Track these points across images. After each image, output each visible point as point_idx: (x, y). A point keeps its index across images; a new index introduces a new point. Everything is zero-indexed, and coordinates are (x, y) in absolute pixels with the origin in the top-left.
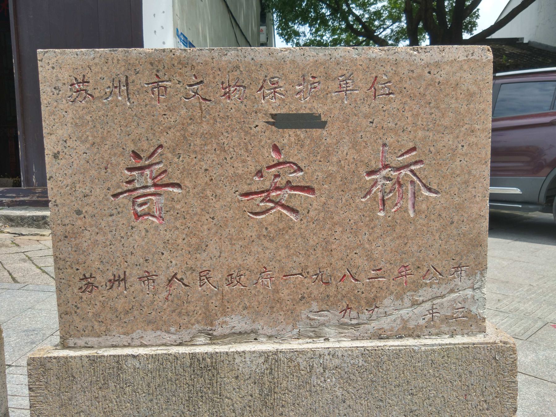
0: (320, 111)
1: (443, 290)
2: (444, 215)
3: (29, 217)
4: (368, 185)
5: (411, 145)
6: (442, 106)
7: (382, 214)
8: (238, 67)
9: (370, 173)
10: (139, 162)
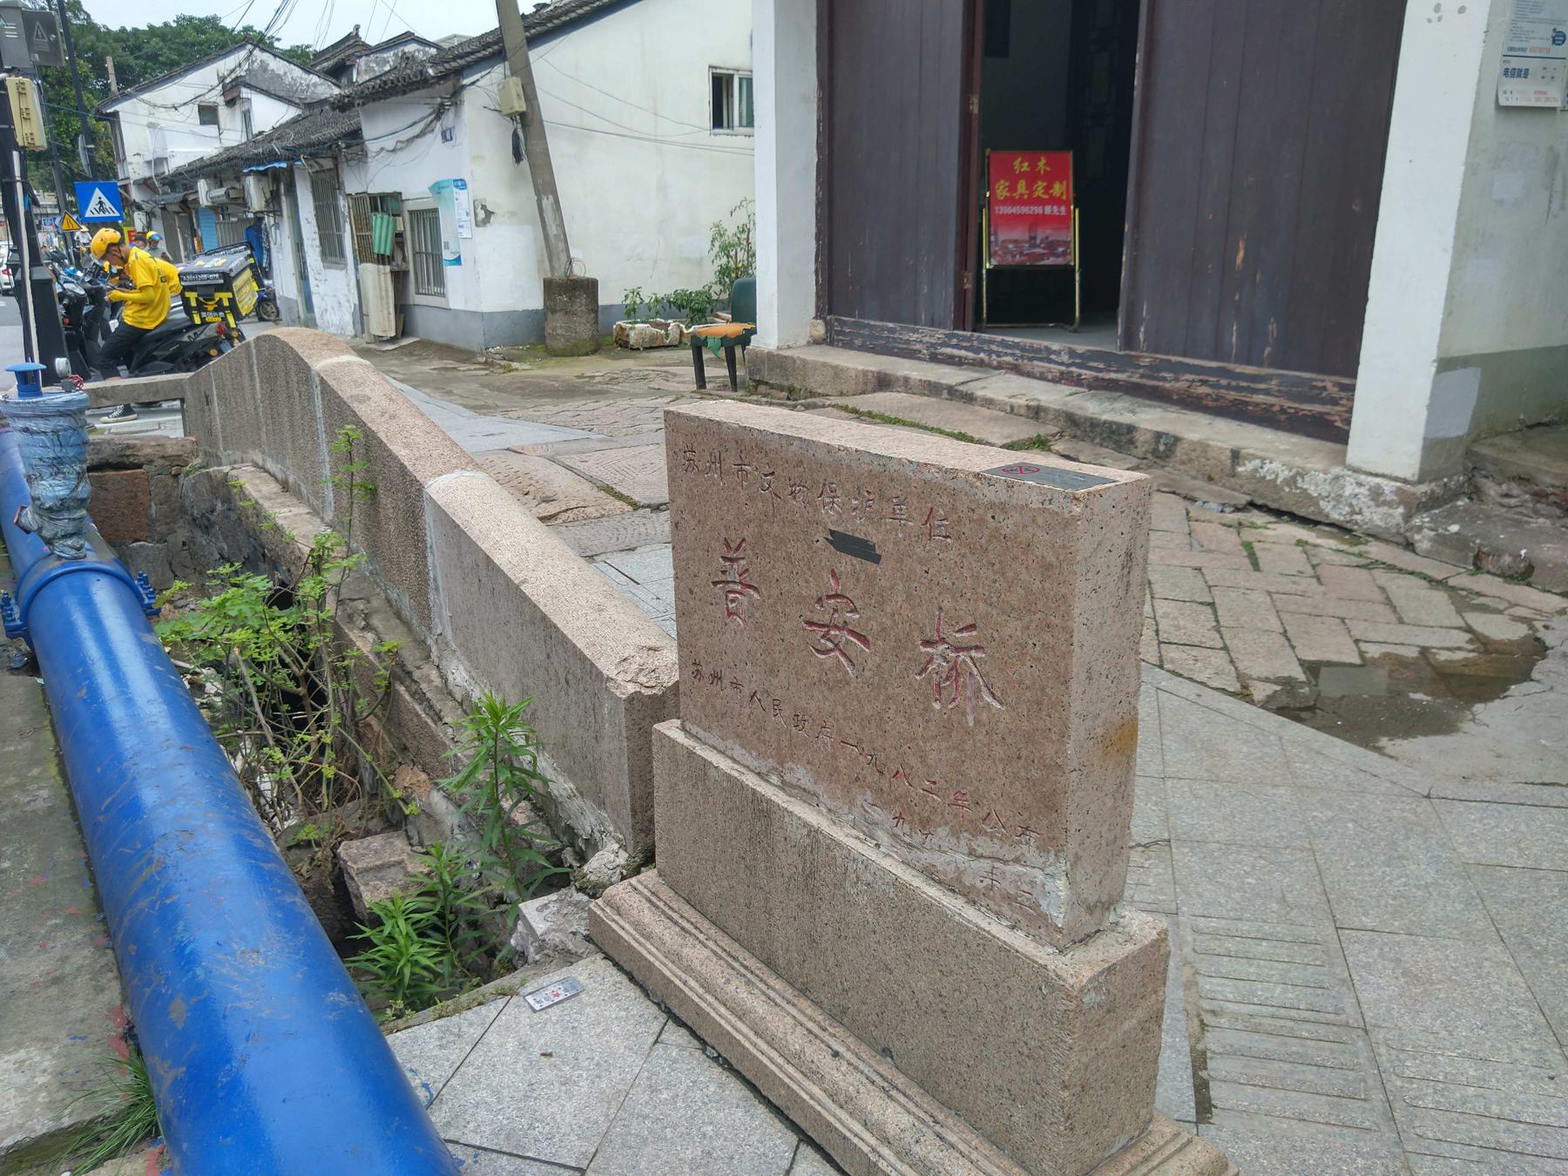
0: (874, 540)
1: (1005, 852)
2: (1009, 741)
3: (1105, 422)
4: (923, 660)
5: (970, 620)
6: (1010, 574)
7: (937, 706)
8: (801, 462)
9: (927, 643)
10: (732, 550)
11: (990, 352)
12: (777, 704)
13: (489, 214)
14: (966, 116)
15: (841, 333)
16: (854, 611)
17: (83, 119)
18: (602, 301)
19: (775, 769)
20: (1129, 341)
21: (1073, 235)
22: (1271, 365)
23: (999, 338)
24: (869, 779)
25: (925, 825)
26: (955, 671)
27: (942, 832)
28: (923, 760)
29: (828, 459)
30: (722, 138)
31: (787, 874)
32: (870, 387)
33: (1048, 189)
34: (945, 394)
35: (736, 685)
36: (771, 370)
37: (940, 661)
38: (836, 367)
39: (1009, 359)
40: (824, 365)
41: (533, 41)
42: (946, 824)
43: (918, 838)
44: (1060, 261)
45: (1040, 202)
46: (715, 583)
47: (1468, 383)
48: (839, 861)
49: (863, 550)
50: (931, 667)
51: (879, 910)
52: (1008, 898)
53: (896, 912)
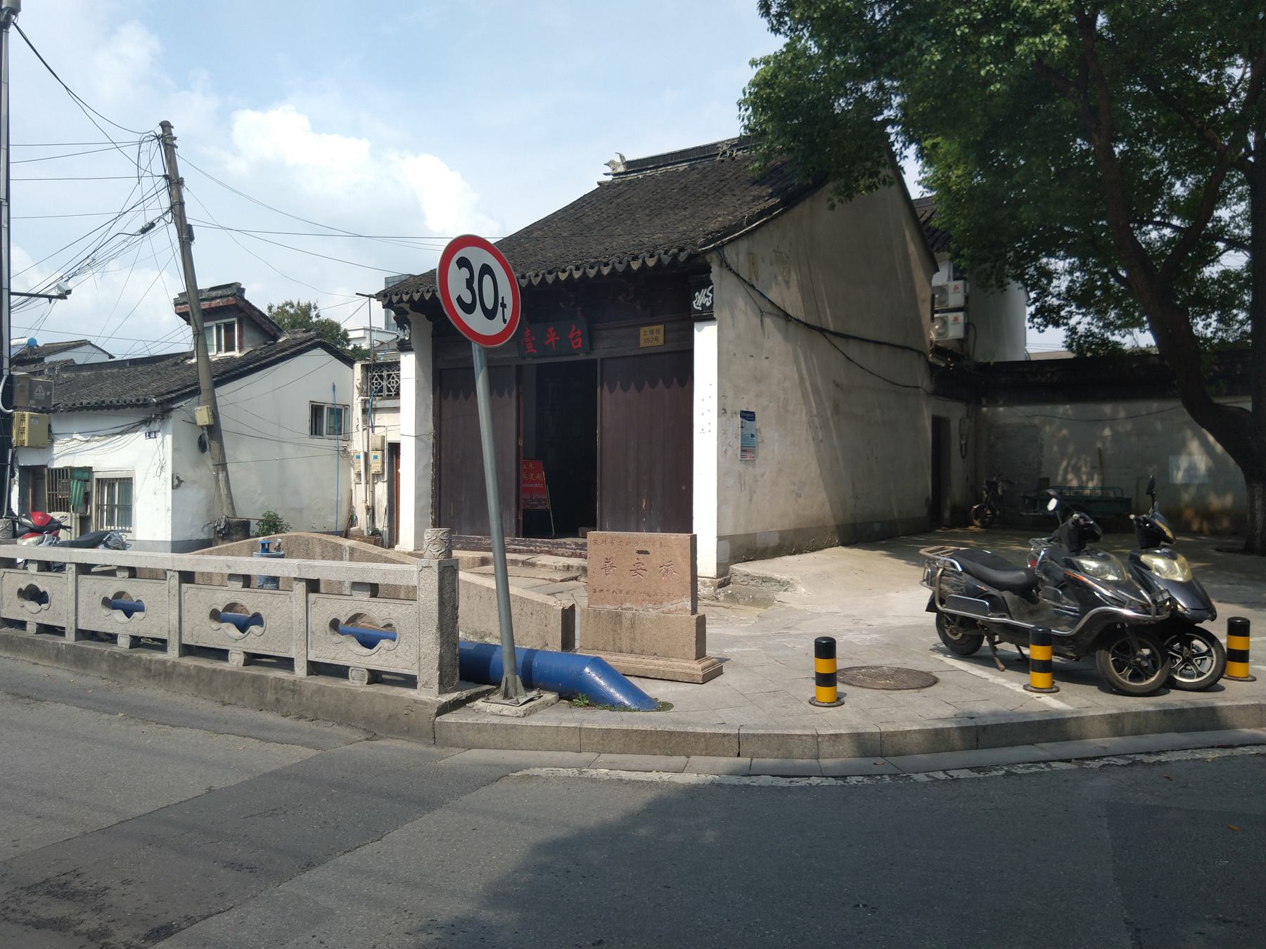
13: (180, 482)
14: (518, 447)
17: (1190, 529)
21: (546, 496)
30: (317, 441)
41: (218, 384)
45: (532, 482)
47: (727, 544)
49: (646, 553)
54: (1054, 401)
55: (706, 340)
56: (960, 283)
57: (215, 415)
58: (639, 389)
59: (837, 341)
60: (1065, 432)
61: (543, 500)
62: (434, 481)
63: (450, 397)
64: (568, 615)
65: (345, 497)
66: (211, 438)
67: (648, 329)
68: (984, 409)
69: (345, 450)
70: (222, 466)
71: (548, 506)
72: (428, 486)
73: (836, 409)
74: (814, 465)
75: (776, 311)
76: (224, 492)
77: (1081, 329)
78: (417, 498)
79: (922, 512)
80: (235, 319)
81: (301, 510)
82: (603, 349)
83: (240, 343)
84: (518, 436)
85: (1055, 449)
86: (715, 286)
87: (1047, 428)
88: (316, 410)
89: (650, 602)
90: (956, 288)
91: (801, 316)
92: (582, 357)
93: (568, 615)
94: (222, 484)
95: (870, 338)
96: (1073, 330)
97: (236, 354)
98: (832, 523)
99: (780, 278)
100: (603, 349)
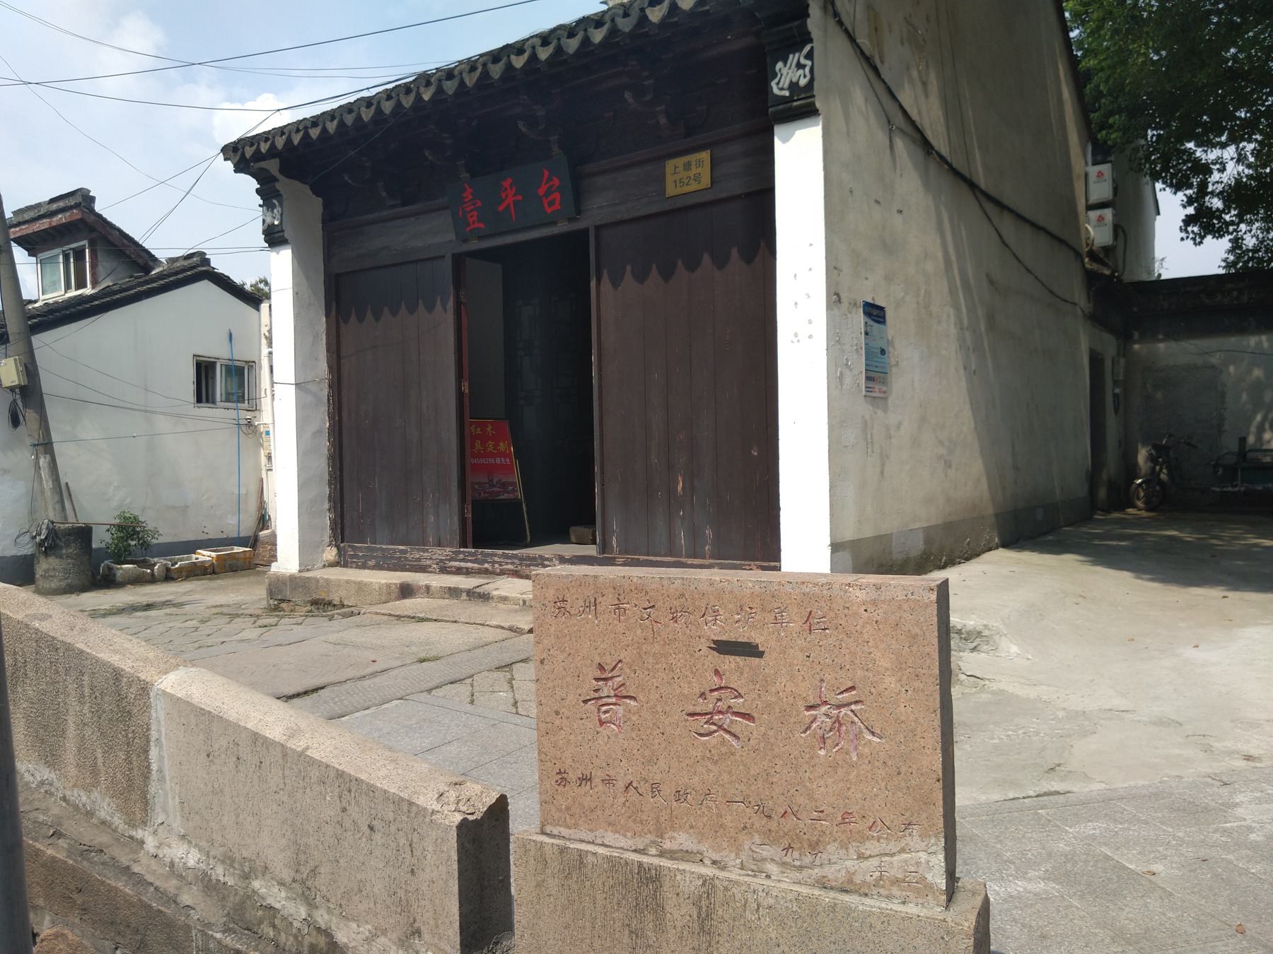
0: (758, 641)
1: (893, 847)
2: (889, 763)
4: (808, 721)
5: (850, 684)
7: (822, 752)
9: (810, 708)
11: (494, 563)
12: (655, 788)
14: (460, 395)
15: (355, 556)
16: (740, 696)
18: (95, 545)
19: (654, 842)
20: (604, 548)
21: (516, 477)
22: (712, 557)
23: (500, 552)
24: (757, 825)
25: (815, 847)
26: (838, 722)
27: (831, 848)
28: (811, 797)
29: (710, 589)
30: (205, 411)
31: (679, 924)
32: (393, 596)
33: (496, 446)
34: (464, 596)
35: (608, 781)
36: (293, 590)
37: (824, 718)
38: (360, 583)
39: (510, 567)
40: (348, 582)
42: (835, 840)
43: (808, 859)
44: (511, 496)
46: (585, 702)
48: (738, 896)
49: (749, 650)
50: (814, 725)
51: (782, 924)
52: (896, 882)
53: (799, 922)
54: (1242, 330)
55: (799, 157)
56: (1106, 168)
57: (30, 369)
58: (667, 274)
59: (989, 207)
60: (1257, 373)
61: (512, 485)
62: (331, 458)
63: (353, 318)
64: (484, 841)
65: (253, 489)
66: (25, 406)
67: (680, 161)
68: (1136, 346)
69: (249, 424)
70: (45, 445)
71: (520, 495)
72: (321, 465)
73: (991, 318)
74: (967, 413)
75: (909, 130)
76: (48, 484)
77: (1250, 242)
78: (302, 486)
79: (1082, 491)
80: (85, 242)
81: (184, 509)
82: (601, 208)
83: (93, 275)
84: (460, 376)
85: (1244, 397)
86: (817, 44)
87: (1232, 369)
88: (204, 369)
89: (770, 837)
90: (1100, 174)
91: (945, 151)
92: (562, 227)
93: (484, 841)
94: (45, 473)
95: (1027, 216)
96: (1237, 243)
97: (88, 291)
98: (990, 510)
99: (915, 73)
100: (601, 208)
